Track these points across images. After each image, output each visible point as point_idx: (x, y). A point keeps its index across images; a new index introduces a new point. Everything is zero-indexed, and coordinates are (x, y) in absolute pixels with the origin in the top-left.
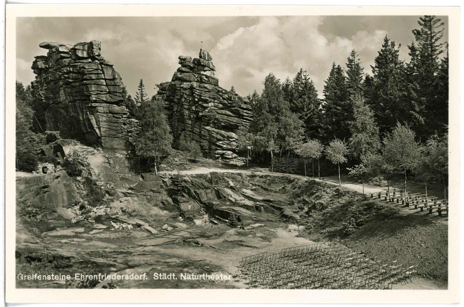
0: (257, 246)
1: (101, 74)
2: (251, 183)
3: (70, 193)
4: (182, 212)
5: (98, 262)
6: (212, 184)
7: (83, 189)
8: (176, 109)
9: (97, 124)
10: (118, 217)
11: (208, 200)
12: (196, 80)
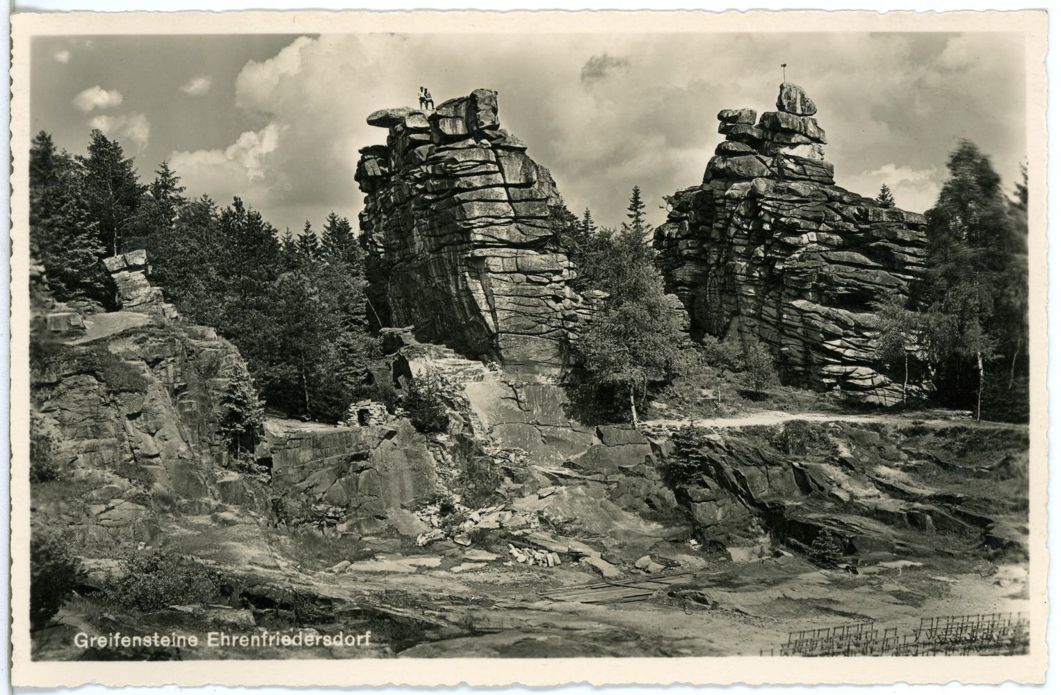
0: (868, 615)
1: (495, 172)
2: (906, 452)
3: (420, 473)
4: (697, 527)
5: (396, 616)
6: (787, 452)
7: (453, 465)
8: (715, 257)
9: (488, 302)
10: (527, 534)
11: (773, 496)
12: (767, 172)
